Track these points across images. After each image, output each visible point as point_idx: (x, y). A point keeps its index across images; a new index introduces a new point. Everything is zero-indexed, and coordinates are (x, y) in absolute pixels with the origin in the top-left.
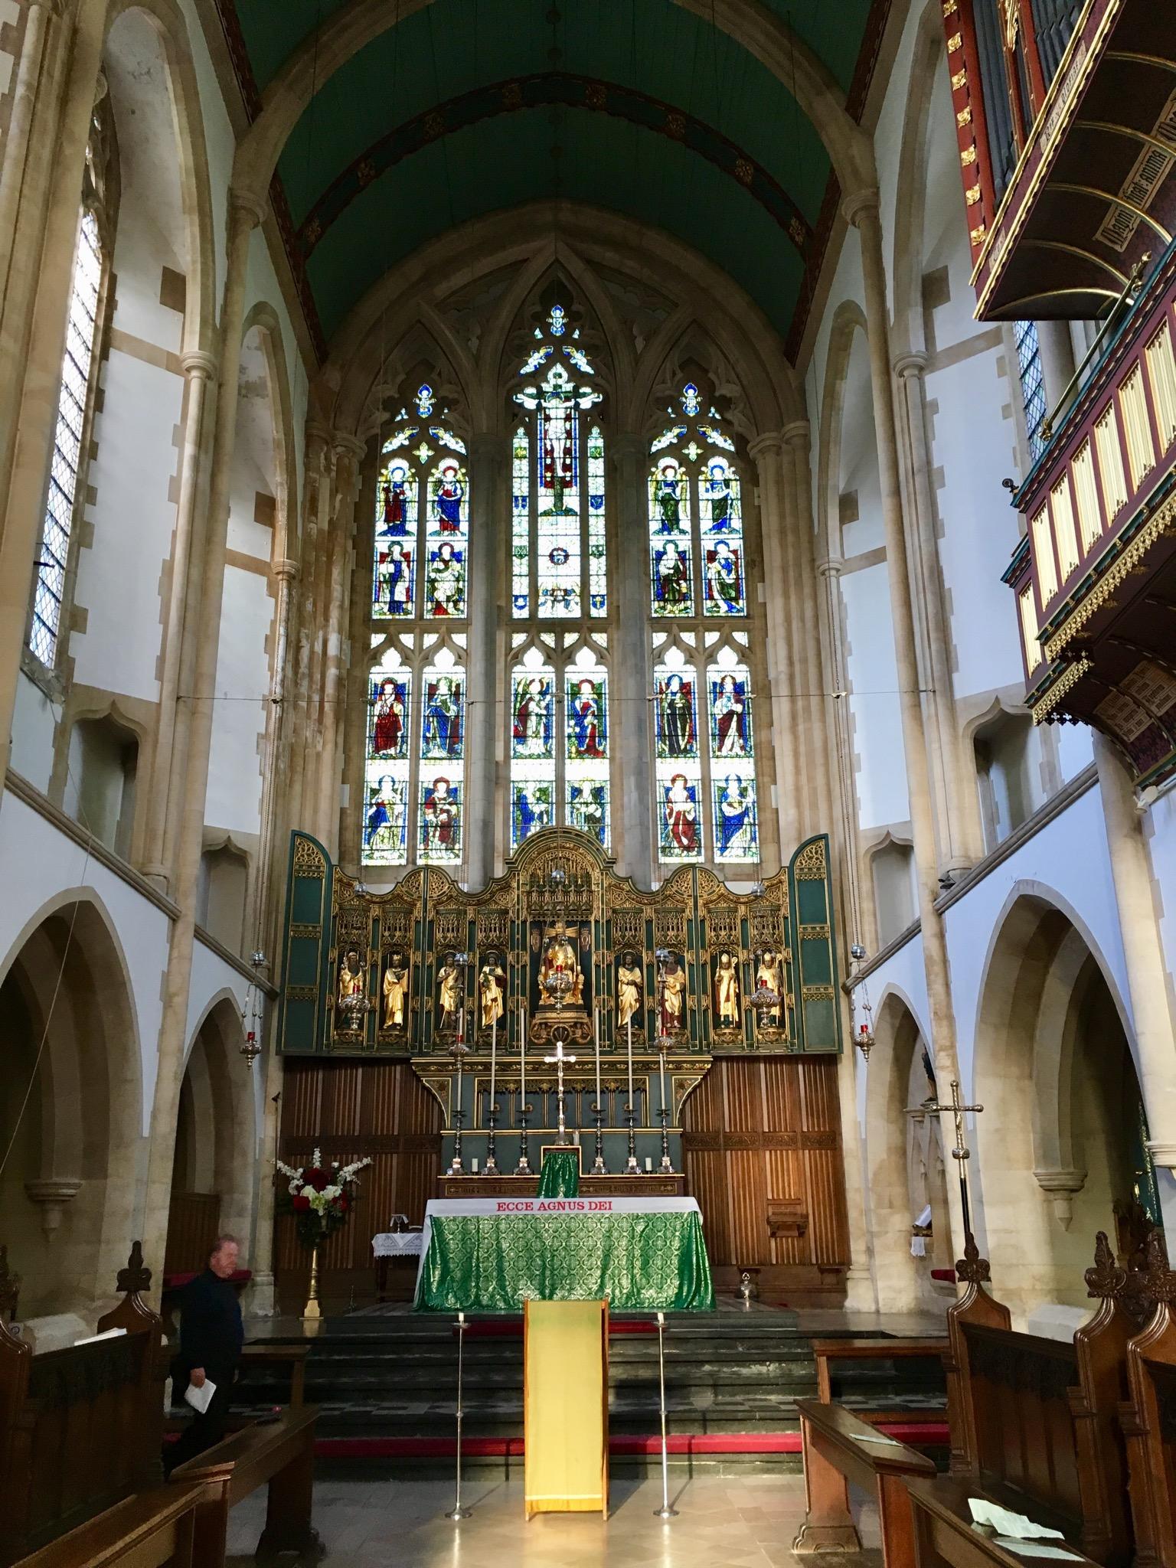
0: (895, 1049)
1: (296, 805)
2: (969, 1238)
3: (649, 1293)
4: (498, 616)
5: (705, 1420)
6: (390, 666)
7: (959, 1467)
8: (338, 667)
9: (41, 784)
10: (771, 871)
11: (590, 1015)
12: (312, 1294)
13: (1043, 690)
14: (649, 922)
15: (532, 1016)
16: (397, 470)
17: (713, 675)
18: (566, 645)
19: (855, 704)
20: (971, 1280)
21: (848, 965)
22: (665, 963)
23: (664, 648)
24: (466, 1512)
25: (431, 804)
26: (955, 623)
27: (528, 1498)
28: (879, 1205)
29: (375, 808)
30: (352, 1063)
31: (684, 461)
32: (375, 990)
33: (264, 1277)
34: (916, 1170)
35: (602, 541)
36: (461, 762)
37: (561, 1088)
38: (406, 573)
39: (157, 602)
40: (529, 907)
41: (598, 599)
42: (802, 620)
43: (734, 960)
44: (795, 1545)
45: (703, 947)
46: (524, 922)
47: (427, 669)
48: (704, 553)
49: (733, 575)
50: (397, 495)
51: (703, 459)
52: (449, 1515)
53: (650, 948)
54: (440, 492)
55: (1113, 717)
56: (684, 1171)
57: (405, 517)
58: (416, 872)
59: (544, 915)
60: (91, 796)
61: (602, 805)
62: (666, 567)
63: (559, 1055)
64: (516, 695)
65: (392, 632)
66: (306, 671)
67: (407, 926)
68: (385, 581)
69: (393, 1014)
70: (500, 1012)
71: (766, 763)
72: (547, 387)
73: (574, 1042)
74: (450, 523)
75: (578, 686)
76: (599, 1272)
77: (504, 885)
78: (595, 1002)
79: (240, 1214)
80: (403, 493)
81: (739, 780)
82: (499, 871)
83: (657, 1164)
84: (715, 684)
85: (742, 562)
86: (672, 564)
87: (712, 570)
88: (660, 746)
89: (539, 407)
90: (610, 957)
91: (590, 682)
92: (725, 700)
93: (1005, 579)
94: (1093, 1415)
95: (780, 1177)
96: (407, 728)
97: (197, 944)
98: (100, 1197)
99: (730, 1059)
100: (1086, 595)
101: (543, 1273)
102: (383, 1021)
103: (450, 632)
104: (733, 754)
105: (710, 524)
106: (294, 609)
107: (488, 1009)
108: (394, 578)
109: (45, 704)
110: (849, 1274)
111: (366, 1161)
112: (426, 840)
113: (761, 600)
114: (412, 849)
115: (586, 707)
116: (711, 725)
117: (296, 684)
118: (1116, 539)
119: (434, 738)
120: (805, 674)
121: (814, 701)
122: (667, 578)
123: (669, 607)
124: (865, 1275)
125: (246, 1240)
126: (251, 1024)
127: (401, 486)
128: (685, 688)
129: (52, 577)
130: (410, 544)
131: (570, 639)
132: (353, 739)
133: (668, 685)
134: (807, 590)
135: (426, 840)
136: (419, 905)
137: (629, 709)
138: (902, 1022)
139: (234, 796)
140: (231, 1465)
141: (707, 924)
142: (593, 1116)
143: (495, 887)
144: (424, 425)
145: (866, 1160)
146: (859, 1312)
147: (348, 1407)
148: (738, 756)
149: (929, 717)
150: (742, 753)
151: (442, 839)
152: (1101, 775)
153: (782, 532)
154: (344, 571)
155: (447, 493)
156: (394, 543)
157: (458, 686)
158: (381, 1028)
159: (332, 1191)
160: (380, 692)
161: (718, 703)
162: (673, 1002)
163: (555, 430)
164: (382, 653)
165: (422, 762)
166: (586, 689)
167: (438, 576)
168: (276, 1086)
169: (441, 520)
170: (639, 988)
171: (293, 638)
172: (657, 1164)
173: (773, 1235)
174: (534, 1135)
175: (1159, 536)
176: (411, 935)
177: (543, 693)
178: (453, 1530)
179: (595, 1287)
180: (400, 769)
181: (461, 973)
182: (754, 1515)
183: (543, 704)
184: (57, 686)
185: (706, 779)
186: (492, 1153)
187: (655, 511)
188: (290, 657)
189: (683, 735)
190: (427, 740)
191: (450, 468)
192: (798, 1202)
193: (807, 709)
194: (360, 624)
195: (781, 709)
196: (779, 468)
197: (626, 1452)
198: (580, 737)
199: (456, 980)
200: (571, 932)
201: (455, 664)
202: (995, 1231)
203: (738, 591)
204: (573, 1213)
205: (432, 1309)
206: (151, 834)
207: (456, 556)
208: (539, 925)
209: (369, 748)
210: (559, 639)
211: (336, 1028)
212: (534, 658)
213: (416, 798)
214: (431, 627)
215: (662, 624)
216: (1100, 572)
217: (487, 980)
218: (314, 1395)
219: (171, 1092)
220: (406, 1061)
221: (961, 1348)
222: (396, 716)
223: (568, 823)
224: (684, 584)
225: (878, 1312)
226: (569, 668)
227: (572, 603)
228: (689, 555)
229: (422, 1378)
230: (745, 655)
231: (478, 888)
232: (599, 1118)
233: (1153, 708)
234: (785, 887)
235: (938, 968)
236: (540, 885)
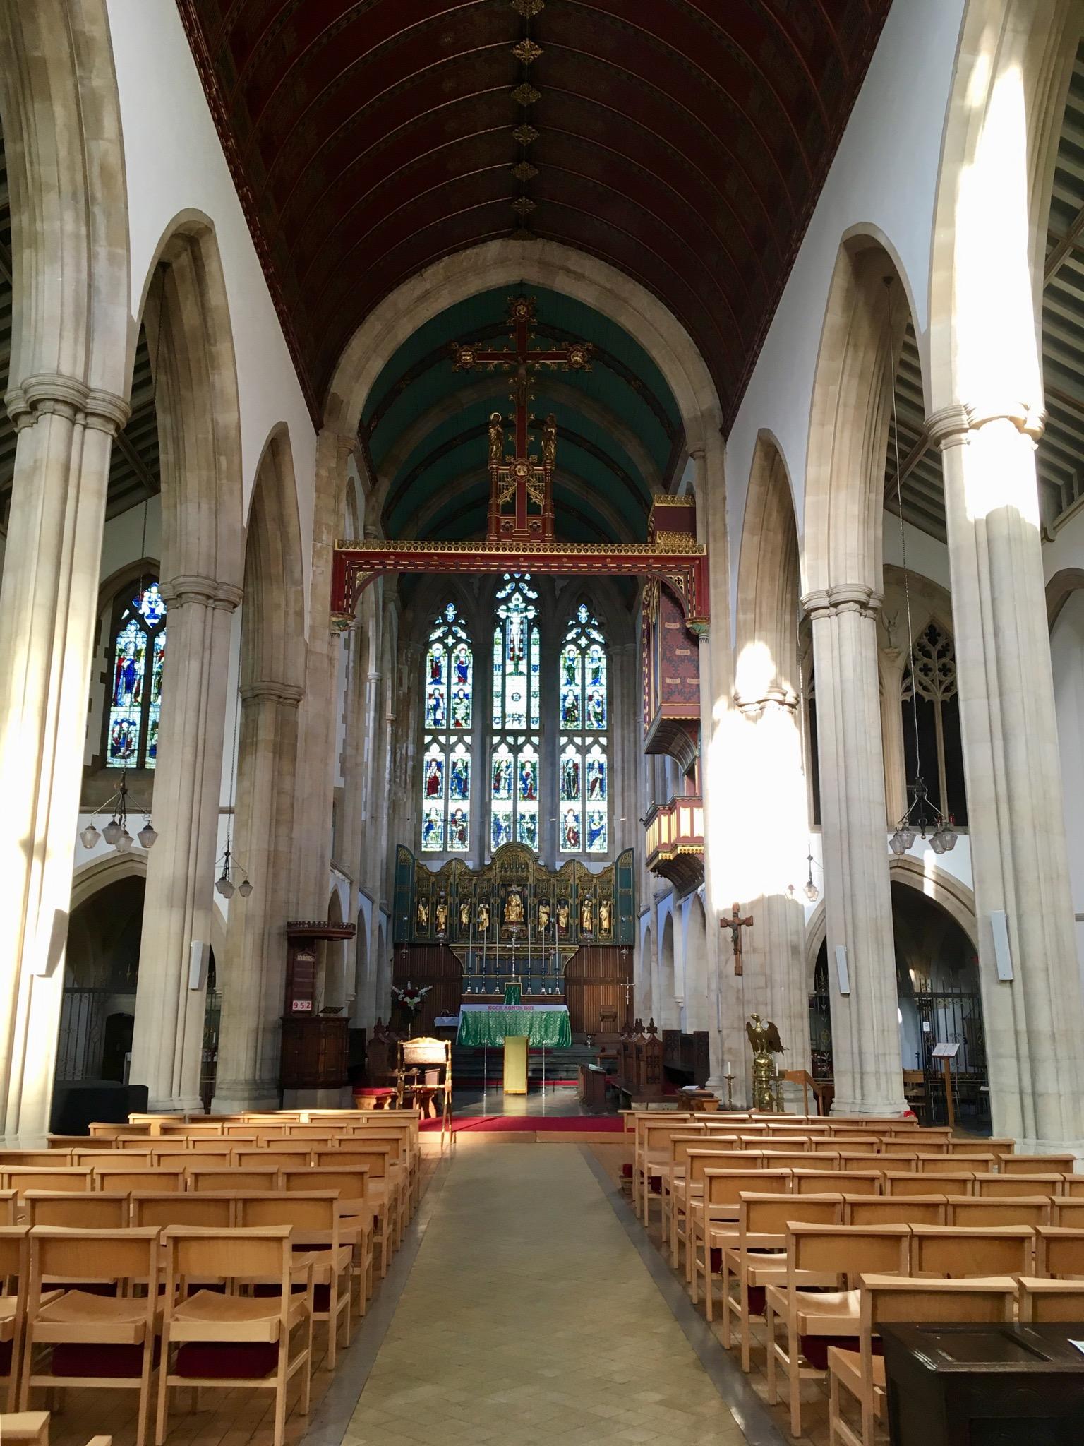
6: (434, 753)
16: (437, 650)
17: (589, 758)
31: (579, 647)
51: (588, 647)
65: (435, 733)
72: (511, 605)
74: (463, 679)
77: (490, 868)
83: (554, 990)
87: (591, 706)
90: (536, 901)
96: (442, 785)
108: (436, 707)
112: (452, 839)
114: (445, 843)
115: (528, 775)
128: (576, 766)
130: (443, 689)
131: (521, 740)
134: (632, 727)
135: (452, 839)
144: (450, 625)
153: (622, 695)
159: (417, 1000)
160: (429, 765)
162: (563, 921)
172: (554, 990)
177: (507, 767)
180: (439, 804)
185: (584, 812)
187: (564, 674)
200: (519, 889)
207: (466, 696)
208: (506, 885)
209: (425, 794)
212: (503, 749)
214: (454, 733)
230: (605, 750)
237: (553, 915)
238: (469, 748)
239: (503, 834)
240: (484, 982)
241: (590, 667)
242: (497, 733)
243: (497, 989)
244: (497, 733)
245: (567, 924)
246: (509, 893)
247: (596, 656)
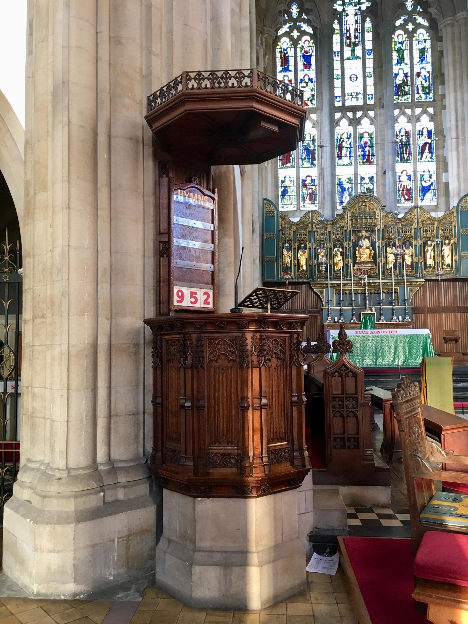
16: (285, 43)
17: (419, 126)
25: (305, 186)
29: (283, 188)
31: (406, 31)
36: (316, 168)
40: (352, 225)
41: (370, 96)
46: (350, 231)
48: (415, 74)
49: (428, 83)
50: (285, 54)
51: (414, 31)
54: (303, 52)
57: (289, 64)
61: (373, 184)
62: (399, 81)
64: (337, 139)
67: (302, 234)
69: (302, 266)
70: (342, 265)
74: (308, 66)
75: (362, 134)
77: (342, 217)
78: (378, 261)
80: (287, 53)
81: (429, 171)
87: (419, 81)
89: (344, 10)
90: (383, 244)
102: (299, 269)
104: (427, 160)
105: (418, 60)
107: (337, 264)
112: (304, 200)
115: (366, 143)
116: (418, 148)
119: (305, 159)
122: (400, 86)
127: (286, 50)
128: (407, 134)
130: (291, 75)
131: (359, 114)
133: (400, 132)
135: (304, 200)
136: (310, 225)
141: (422, 229)
144: (295, 21)
148: (428, 161)
151: (310, 199)
153: (454, 63)
155: (306, 52)
156: (285, 76)
157: (314, 137)
158: (298, 271)
161: (421, 139)
163: (351, 21)
166: (366, 135)
169: (304, 64)
172: (404, 319)
177: (348, 138)
180: (292, 172)
183: (348, 143)
185: (415, 172)
187: (395, 55)
189: (406, 153)
190: (302, 160)
191: (306, 40)
192: (455, 331)
196: (453, 33)
198: (364, 156)
200: (368, 234)
201: (313, 127)
203: (429, 90)
207: (311, 80)
217: (336, 253)
226: (359, 127)
228: (409, 74)
230: (432, 118)
234: (455, 214)
239: (346, 194)
241: (417, 47)
242: (338, 109)
244: (338, 109)
246: (359, 238)
247: (421, 38)
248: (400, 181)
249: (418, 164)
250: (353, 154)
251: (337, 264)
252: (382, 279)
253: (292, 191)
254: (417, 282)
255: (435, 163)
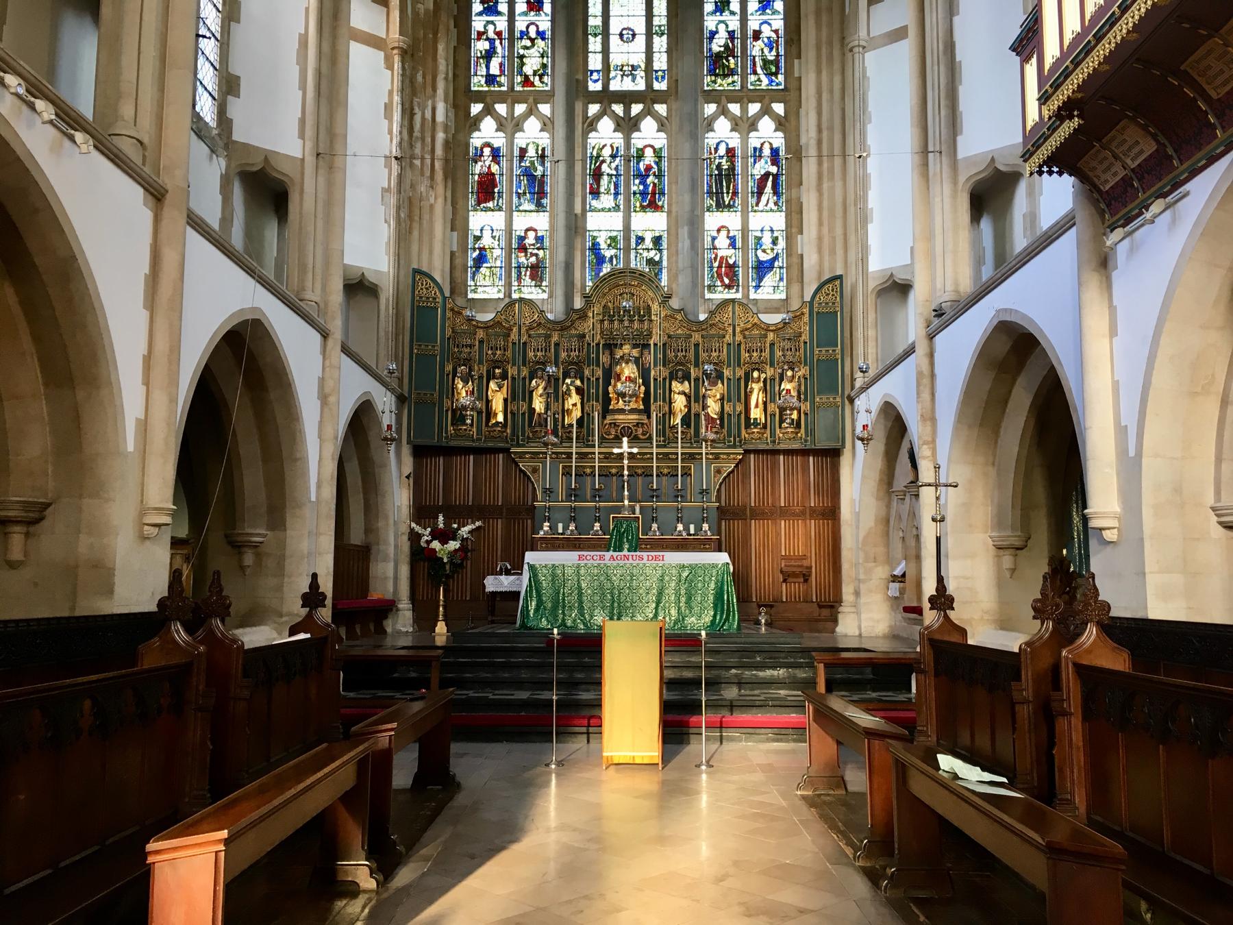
0: (887, 444)
1: (415, 248)
2: (940, 579)
3: (691, 620)
4: (576, 90)
5: (732, 706)
6: (487, 132)
7: (922, 739)
8: (446, 132)
9: (214, 221)
10: (795, 305)
11: (649, 417)
12: (441, 618)
13: (1037, 146)
14: (697, 345)
15: (604, 417)
18: (633, 114)
19: (872, 165)
20: (939, 609)
21: (853, 380)
22: (708, 376)
23: (714, 118)
24: (560, 764)
25: (523, 248)
26: (963, 92)
27: (605, 754)
28: (866, 560)
30: (466, 451)
32: (481, 393)
33: (405, 605)
34: (896, 536)
35: (664, 21)
36: (547, 214)
37: (626, 472)
38: (499, 49)
39: (295, 71)
40: (602, 332)
42: (831, 91)
43: (763, 376)
44: (798, 788)
45: (739, 365)
46: (598, 345)
47: (518, 135)
48: (750, 33)
49: (774, 53)
52: (548, 765)
53: (697, 365)
55: (1094, 168)
56: (719, 534)
58: (512, 303)
59: (614, 339)
60: (253, 235)
61: (660, 251)
62: (717, 46)
63: (625, 447)
65: (489, 100)
66: (419, 135)
67: (506, 346)
68: (482, 57)
69: (496, 414)
70: (579, 414)
71: (795, 216)
73: (636, 438)
75: (642, 150)
76: (654, 605)
77: (582, 315)
78: (653, 408)
79: (386, 559)
81: (772, 231)
82: (578, 303)
83: (699, 529)
84: (755, 149)
85: (782, 41)
86: (722, 42)
87: (757, 48)
88: (709, 202)
90: (665, 373)
91: (652, 146)
92: (763, 161)
93: (1013, 48)
94: (1030, 702)
95: (792, 539)
96: (502, 185)
97: (343, 356)
98: (282, 545)
99: (757, 452)
100: (1084, 59)
101: (612, 605)
102: (488, 420)
103: (536, 102)
104: (768, 208)
106: (407, 81)
107: (569, 412)
108: (489, 55)
109: (211, 158)
110: (840, 609)
111: (478, 524)
112: (519, 278)
113: (796, 75)
114: (509, 285)
115: (649, 168)
117: (411, 146)
118: (1115, 8)
119: (525, 193)
120: (831, 140)
121: (838, 161)
122: (719, 55)
123: (719, 81)
124: (853, 609)
125: (391, 575)
126: (387, 419)
128: (731, 153)
129: (209, 47)
130: (502, 24)
131: (636, 109)
132: (459, 195)
133: (716, 149)
134: (837, 66)
135: (519, 278)
136: (515, 329)
137: (685, 168)
138: (894, 424)
139: (366, 240)
140: (395, 725)
141: (743, 346)
142: (651, 493)
143: (575, 316)
145: (858, 527)
146: (846, 636)
147: (471, 694)
148: (771, 210)
149: (935, 174)
150: (775, 208)
151: (532, 278)
152: (1077, 220)
153: (818, 13)
154: (447, 49)
156: (488, 22)
157: (543, 149)
158: (487, 425)
159: (453, 545)
160: (479, 156)
161: (757, 165)
162: (713, 407)
164: (481, 121)
165: (515, 214)
166: (649, 152)
167: (526, 52)
168: (408, 467)
170: (688, 397)
171: (407, 106)
172: (699, 529)
173: (785, 581)
174: (605, 507)
175: (1123, 38)
176: (509, 353)
177: (613, 156)
178: (550, 773)
179: (651, 615)
180: (496, 220)
181: (549, 381)
182: (767, 768)
183: (613, 165)
184: (221, 143)
185: (745, 230)
186: (573, 519)
188: (406, 123)
190: (519, 195)
192: (804, 557)
193: (831, 170)
194: (462, 95)
195: (810, 168)
197: (676, 724)
198: (643, 194)
199: (545, 389)
200: (635, 353)
202: (956, 578)
203: (778, 68)
204: (635, 563)
205: (530, 628)
206: (303, 268)
207: (541, 35)
208: (610, 347)
209: (472, 201)
210: (628, 107)
211: (452, 424)
212: (606, 125)
213: (511, 244)
215: (712, 96)
216: (1099, 38)
217: (569, 389)
218: (444, 684)
219: (331, 468)
220: (506, 451)
221: (929, 658)
222: (493, 174)
223: (633, 265)
224: (732, 61)
225: (860, 635)
226: (635, 135)
227: (638, 78)
228: (738, 34)
229: (524, 675)
230: (781, 124)
231: (561, 317)
232: (654, 494)
233: (1129, 161)
234: (806, 318)
235: (926, 381)
236: (609, 315)
237: (695, 398)
238: (547, 124)
240: (573, 516)
243: (597, 526)
245: (721, 414)
246: (614, 362)
248: (715, 248)
249: (751, 214)
250: (622, 190)
251: (569, 412)
252: (658, 446)
253: (497, 255)
254: (728, 454)
255: (783, 214)
